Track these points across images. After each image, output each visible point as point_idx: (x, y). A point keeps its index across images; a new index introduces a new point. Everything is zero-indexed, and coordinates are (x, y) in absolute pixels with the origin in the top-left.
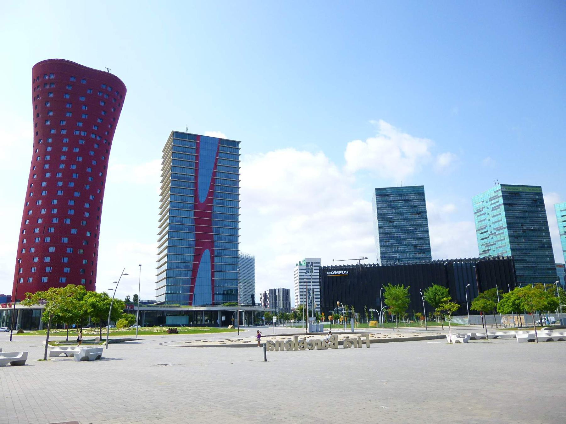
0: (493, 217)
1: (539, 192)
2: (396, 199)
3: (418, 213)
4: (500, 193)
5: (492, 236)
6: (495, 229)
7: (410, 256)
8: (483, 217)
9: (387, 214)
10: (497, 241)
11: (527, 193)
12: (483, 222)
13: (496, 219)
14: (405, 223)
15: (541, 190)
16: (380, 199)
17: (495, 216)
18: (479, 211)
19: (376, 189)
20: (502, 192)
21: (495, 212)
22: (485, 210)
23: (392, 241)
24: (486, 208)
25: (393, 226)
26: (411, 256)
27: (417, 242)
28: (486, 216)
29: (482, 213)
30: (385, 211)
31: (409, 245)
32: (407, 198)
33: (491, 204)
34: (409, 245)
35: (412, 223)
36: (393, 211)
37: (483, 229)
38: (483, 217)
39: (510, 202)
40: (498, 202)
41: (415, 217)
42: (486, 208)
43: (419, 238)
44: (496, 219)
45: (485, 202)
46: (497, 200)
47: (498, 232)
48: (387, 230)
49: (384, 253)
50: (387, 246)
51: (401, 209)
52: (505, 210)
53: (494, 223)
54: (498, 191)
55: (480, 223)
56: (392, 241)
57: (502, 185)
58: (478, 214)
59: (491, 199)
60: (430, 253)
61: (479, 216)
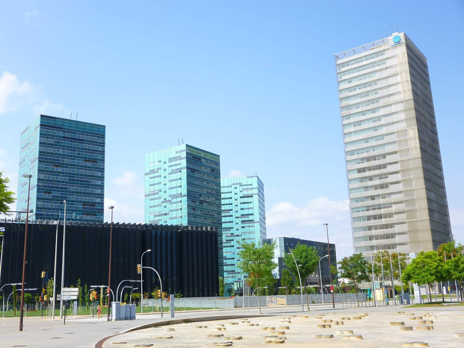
0: (171, 181)
1: (217, 161)
2: (67, 135)
3: (95, 161)
4: (184, 155)
5: (165, 204)
6: (170, 196)
7: (76, 217)
8: (157, 180)
9: (52, 154)
10: (171, 211)
11: (207, 160)
12: (156, 186)
13: (174, 184)
14: (75, 171)
15: (219, 160)
16: (45, 131)
17: (173, 180)
18: (152, 172)
19: (42, 116)
20: (187, 153)
21: (174, 176)
22: (161, 172)
23: (55, 193)
24: (162, 170)
25: (59, 172)
26: (78, 217)
27: (87, 199)
28: (161, 180)
29: (156, 174)
30: (51, 150)
31: (77, 202)
32: (82, 137)
33: (170, 166)
34: (77, 202)
35: (82, 172)
36: (61, 151)
37: (154, 194)
38: (157, 180)
39: (192, 166)
40: (180, 164)
41: (89, 164)
42: (162, 170)
43: (89, 194)
44: (174, 184)
45: (162, 162)
46: (178, 162)
47: (174, 200)
48: (48, 177)
49: (42, 208)
50: (46, 199)
51: (70, 151)
52: (188, 176)
53: (171, 188)
54: (181, 151)
55: (152, 187)
56: (55, 193)
57: (187, 146)
58: (151, 176)
59: (171, 160)
60: (103, 216)
61: (151, 178)
